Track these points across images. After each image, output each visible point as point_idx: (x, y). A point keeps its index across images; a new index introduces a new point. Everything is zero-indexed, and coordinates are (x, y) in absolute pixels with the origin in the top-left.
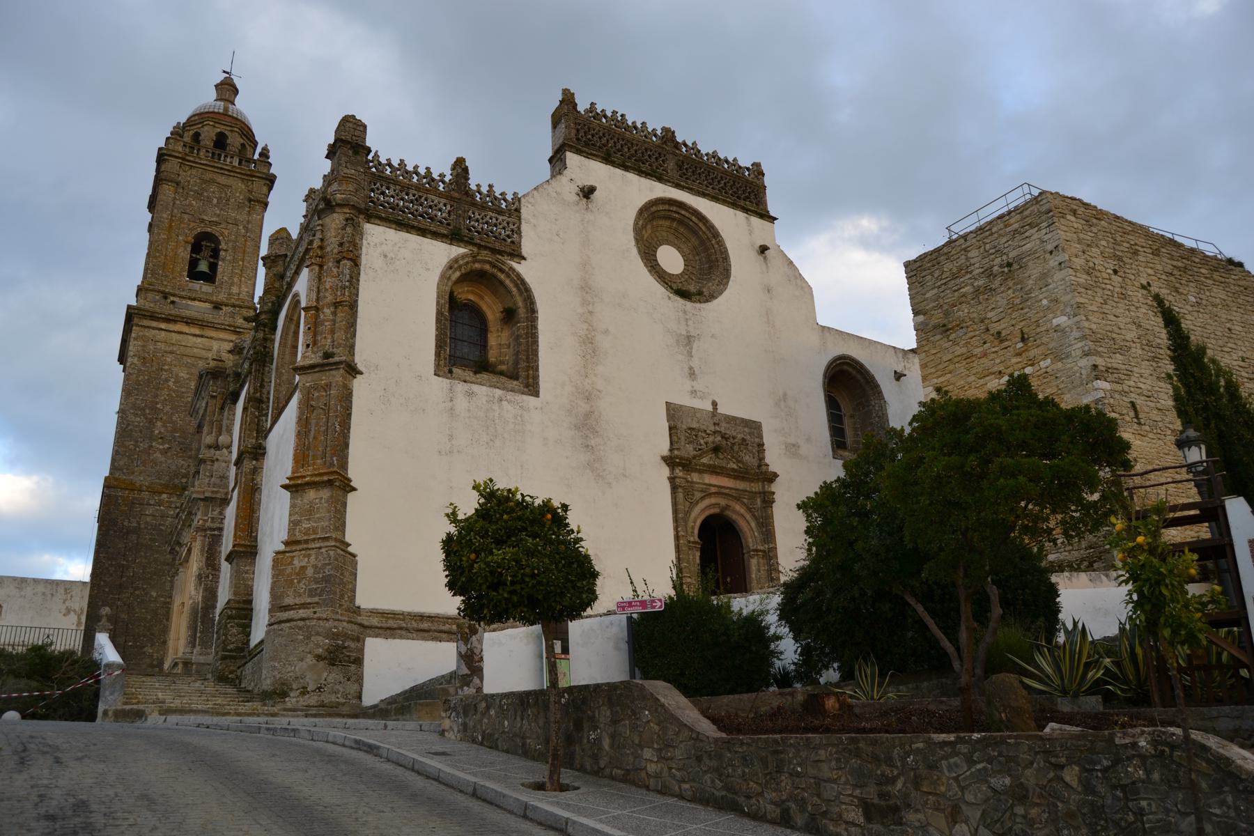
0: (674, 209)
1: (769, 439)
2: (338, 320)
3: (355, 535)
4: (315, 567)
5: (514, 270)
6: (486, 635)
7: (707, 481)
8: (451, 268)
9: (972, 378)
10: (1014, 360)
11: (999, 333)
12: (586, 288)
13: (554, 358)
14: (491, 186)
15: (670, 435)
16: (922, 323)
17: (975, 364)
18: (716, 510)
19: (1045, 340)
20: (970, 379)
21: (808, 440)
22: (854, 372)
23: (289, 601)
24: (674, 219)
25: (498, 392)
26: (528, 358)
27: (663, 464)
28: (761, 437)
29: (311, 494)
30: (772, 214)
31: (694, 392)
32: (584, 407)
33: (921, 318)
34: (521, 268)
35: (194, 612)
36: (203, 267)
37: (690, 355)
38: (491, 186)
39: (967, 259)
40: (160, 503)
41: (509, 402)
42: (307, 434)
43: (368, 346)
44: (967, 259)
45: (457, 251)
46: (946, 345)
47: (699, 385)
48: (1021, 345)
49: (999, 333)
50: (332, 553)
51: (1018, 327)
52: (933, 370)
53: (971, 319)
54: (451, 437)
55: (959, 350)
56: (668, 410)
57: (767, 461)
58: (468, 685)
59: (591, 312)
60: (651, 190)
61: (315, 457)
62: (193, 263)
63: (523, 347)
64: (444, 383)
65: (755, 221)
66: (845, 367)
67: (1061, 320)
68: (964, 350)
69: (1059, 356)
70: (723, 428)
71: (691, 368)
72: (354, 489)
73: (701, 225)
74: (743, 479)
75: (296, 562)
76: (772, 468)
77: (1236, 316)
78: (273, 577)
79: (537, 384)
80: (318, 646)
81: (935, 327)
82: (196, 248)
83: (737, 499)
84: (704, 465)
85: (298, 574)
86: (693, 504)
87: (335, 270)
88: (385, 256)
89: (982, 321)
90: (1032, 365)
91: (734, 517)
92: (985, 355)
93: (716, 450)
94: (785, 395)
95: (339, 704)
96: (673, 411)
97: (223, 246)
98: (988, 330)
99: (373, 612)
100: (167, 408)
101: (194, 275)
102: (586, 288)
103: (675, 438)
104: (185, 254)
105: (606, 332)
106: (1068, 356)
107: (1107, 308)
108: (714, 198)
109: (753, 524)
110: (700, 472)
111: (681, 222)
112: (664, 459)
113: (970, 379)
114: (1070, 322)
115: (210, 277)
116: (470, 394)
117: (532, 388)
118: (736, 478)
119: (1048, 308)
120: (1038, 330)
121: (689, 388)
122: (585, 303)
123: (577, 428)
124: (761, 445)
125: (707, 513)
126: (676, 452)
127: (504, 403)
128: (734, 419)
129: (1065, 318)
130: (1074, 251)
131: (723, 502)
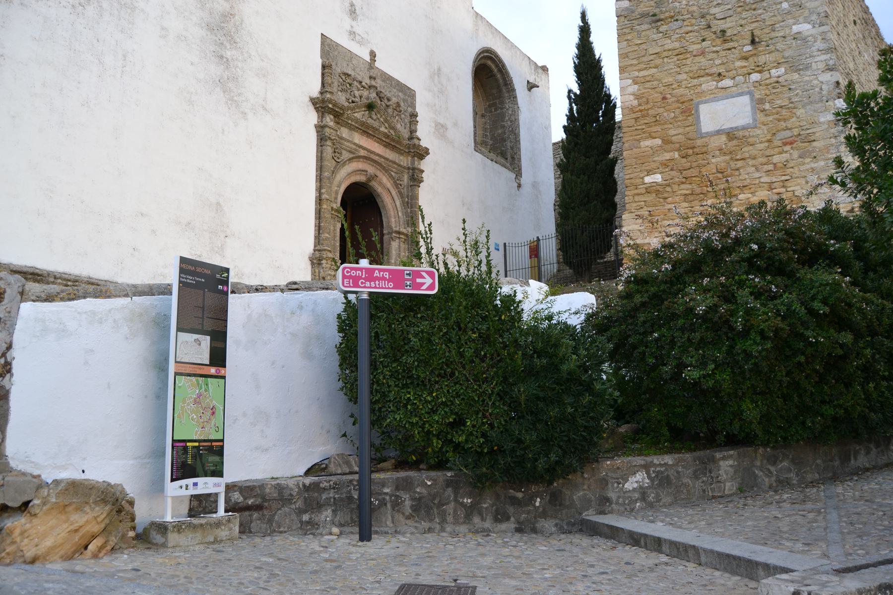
6: (26, 308)
7: (357, 141)
9: (684, 76)
10: (739, 64)
11: (723, 32)
15: (323, 74)
17: (688, 62)
18: (361, 178)
19: (780, 46)
20: (680, 77)
21: (455, 124)
22: (496, 70)
27: (312, 108)
28: (413, 106)
31: (352, 34)
46: (655, 37)
48: (749, 48)
49: (723, 32)
51: (747, 28)
52: (635, 62)
53: (689, 12)
55: (669, 44)
56: (323, 44)
57: (419, 134)
66: (489, 63)
67: (804, 28)
68: (677, 45)
69: (795, 66)
70: (378, 83)
74: (393, 148)
76: (424, 143)
81: (643, 15)
83: (385, 170)
84: (357, 120)
86: (339, 164)
89: (703, 17)
90: (760, 72)
91: (379, 190)
92: (703, 53)
93: (370, 107)
94: (439, 69)
96: (328, 47)
98: (709, 27)
103: (328, 80)
106: (807, 67)
109: (398, 203)
110: (351, 128)
112: (314, 101)
113: (680, 77)
114: (814, 31)
118: (387, 145)
119: (789, 13)
120: (773, 35)
121: (349, 28)
123: (210, 28)
124: (414, 115)
126: (328, 96)
129: (809, 26)
131: (371, 170)
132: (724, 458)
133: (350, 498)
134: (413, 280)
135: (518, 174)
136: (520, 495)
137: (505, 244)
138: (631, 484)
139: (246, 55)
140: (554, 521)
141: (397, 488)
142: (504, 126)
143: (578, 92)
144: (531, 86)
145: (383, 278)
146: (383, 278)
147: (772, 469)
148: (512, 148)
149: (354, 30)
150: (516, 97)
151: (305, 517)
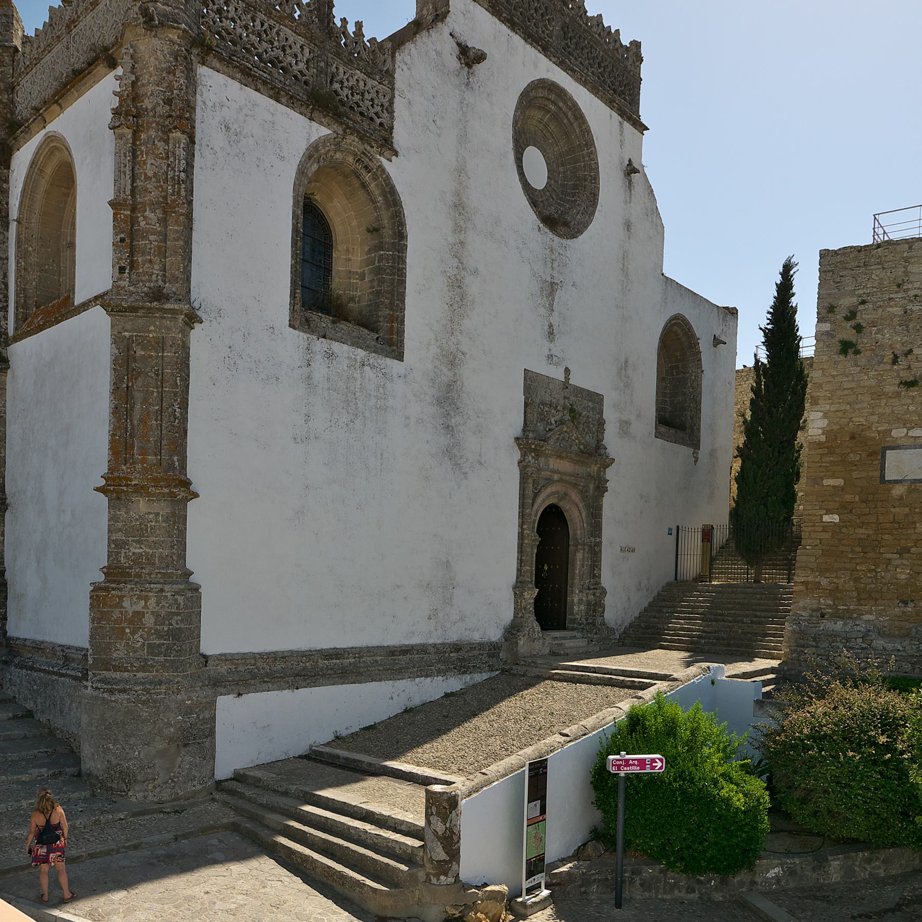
0: (552, 97)
1: (609, 414)
2: (171, 236)
3: (198, 560)
4: (156, 615)
5: (384, 171)
8: (310, 157)
12: (459, 207)
14: (359, 25)
15: (525, 412)
16: (827, 333)
21: (639, 416)
24: (548, 111)
25: (361, 353)
26: (392, 303)
30: (644, 120)
33: (827, 327)
34: (392, 167)
38: (359, 25)
39: (906, 273)
41: (372, 367)
42: (129, 412)
43: (209, 278)
44: (906, 273)
45: (320, 131)
50: (180, 599)
58: (446, 875)
59: (462, 243)
61: (144, 452)
63: (385, 287)
64: (299, 337)
65: (627, 126)
71: (551, 326)
72: (196, 495)
73: (575, 125)
75: (126, 604)
78: (93, 620)
79: (402, 341)
80: (169, 725)
85: (131, 622)
87: (160, 145)
88: (228, 128)
95: (195, 792)
98: (909, 368)
99: (224, 658)
102: (459, 207)
108: (594, 90)
109: (584, 515)
111: (555, 117)
117: (393, 346)
121: (547, 352)
122: (458, 229)
125: (547, 504)
127: (367, 368)
132: (834, 860)
133: (607, 879)
134: (651, 764)
135: (694, 443)
136: (702, 878)
137: (678, 527)
138: (771, 874)
139: (466, 417)
140: (721, 894)
141: (633, 874)
142: (685, 394)
143: (765, 361)
144: (717, 342)
145: (634, 765)
146: (634, 765)
147: (867, 866)
148: (692, 418)
149: (552, 352)
150: (700, 360)
151: (583, 889)
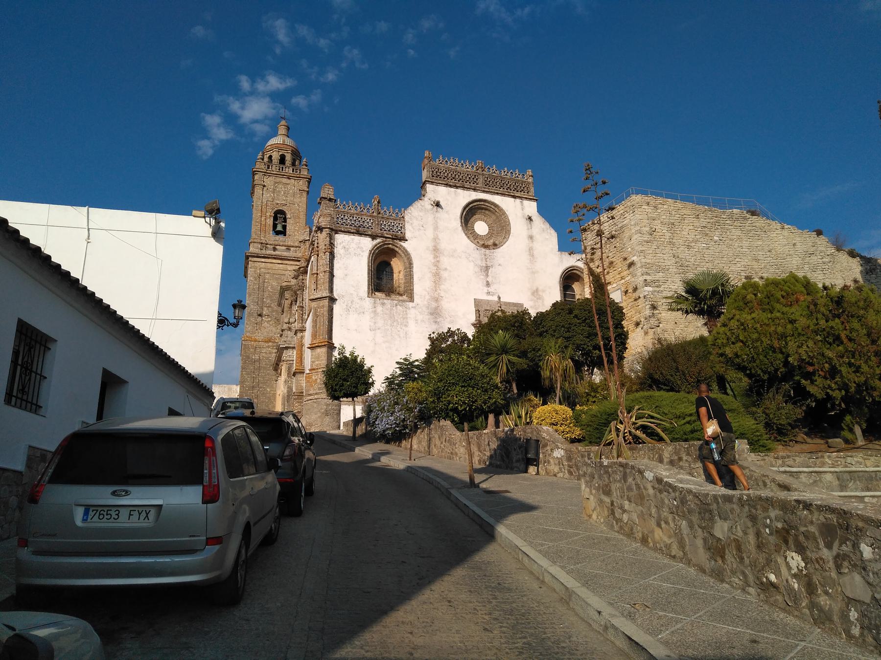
13: (421, 286)
23: (311, 392)
29: (319, 350)
32: (434, 305)
35: (283, 398)
36: (279, 228)
37: (487, 275)
40: (268, 347)
47: (491, 289)
54: (375, 323)
60: (470, 196)
62: (275, 226)
77: (745, 244)
82: (275, 218)
97: (288, 216)
100: (268, 301)
101: (278, 233)
104: (270, 222)
105: (446, 269)
107: (658, 251)
115: (283, 233)
116: (383, 304)
122: (436, 257)
123: (431, 314)
128: (509, 303)
130: (644, 224)
